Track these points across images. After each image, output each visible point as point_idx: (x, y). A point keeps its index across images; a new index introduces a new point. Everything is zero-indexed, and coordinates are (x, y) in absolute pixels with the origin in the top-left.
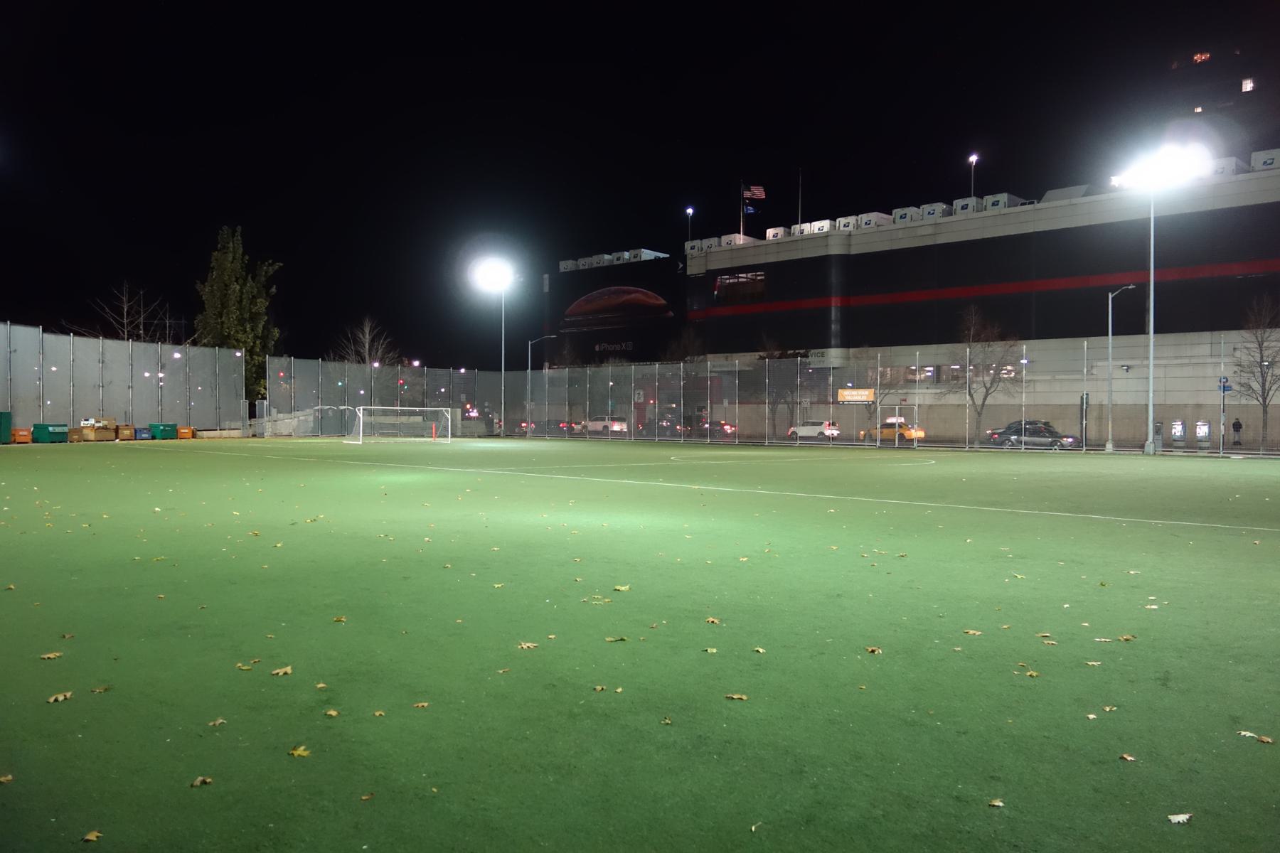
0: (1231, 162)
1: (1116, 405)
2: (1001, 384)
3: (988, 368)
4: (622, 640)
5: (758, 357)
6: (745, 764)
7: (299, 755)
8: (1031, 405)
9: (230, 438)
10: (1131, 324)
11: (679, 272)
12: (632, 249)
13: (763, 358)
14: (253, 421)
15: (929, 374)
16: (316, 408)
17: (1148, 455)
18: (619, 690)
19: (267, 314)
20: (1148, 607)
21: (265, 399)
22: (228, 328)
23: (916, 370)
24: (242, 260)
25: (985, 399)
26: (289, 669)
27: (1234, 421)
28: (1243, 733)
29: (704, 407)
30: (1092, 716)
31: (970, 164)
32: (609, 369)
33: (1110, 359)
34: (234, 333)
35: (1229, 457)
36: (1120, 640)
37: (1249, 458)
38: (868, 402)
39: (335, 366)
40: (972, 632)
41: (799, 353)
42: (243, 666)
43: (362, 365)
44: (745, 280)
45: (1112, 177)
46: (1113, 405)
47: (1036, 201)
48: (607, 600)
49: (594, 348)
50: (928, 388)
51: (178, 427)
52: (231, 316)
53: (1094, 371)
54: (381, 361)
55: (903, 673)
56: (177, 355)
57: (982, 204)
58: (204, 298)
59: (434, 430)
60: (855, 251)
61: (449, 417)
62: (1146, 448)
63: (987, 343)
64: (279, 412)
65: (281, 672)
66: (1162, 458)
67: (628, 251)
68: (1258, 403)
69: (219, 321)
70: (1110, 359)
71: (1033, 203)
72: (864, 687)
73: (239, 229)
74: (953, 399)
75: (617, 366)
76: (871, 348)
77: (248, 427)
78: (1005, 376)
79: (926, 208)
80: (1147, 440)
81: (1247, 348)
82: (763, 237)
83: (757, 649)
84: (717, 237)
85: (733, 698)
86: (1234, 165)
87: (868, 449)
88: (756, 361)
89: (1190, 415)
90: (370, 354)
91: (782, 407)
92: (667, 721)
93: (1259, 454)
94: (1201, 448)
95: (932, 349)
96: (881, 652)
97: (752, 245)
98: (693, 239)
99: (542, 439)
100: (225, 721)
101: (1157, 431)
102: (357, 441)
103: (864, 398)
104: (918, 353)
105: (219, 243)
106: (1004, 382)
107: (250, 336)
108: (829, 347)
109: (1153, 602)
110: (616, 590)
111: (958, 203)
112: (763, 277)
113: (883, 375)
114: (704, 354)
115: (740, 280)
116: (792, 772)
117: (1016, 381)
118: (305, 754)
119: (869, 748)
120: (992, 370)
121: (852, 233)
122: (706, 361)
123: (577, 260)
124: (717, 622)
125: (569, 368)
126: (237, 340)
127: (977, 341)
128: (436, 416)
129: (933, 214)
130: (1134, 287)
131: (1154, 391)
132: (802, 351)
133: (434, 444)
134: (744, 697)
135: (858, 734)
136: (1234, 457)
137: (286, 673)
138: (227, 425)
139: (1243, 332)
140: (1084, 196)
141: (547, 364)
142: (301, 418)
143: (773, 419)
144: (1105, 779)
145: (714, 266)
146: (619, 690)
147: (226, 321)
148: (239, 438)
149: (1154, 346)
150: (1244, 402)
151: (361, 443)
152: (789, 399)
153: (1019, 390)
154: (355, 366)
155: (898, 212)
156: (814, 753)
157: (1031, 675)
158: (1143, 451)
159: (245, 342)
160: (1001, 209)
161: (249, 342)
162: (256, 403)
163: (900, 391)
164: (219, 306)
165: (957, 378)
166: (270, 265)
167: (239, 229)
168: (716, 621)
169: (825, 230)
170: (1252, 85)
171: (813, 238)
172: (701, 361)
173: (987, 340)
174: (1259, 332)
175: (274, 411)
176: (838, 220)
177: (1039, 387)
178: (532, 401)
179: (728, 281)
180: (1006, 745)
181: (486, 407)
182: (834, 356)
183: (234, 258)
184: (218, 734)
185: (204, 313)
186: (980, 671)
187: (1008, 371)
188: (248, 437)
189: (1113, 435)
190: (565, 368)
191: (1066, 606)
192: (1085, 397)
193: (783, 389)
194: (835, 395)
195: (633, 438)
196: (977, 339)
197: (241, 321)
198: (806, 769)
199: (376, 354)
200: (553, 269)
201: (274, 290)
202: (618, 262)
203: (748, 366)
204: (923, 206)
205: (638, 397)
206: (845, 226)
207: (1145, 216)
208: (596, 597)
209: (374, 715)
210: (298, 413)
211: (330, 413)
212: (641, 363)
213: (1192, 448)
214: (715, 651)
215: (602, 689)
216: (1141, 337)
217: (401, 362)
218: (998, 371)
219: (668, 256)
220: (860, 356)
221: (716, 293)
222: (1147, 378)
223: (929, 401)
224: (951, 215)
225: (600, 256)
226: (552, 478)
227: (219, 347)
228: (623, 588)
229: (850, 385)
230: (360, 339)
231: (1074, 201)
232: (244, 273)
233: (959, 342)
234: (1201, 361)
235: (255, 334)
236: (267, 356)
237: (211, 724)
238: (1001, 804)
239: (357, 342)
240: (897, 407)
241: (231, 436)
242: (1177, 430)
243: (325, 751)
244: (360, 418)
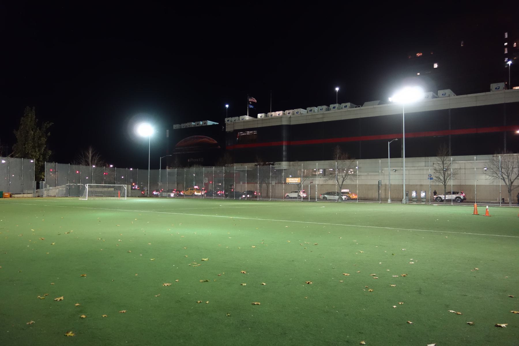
0: (431, 94)
1: (392, 185)
2: (349, 176)
3: (343, 170)
4: (207, 281)
5: (254, 165)
6: (262, 331)
7: (69, 336)
8: (360, 185)
9: (27, 197)
10: (396, 154)
11: (222, 130)
12: (196, 121)
13: (256, 165)
14: (38, 190)
15: (321, 172)
16: (67, 185)
17: (404, 204)
18: (207, 302)
19: (46, 144)
20: (411, 263)
21: (44, 180)
22: (28, 150)
23: (316, 171)
24: (35, 121)
25: (343, 182)
26: (62, 298)
27: (434, 191)
28: (451, 311)
29: (233, 185)
30: (395, 307)
31: (336, 92)
32: (194, 170)
33: (389, 167)
34: (31, 152)
35: (433, 205)
36: (401, 276)
37: (439, 205)
38: (298, 183)
39: (76, 167)
40: (346, 274)
41: (271, 163)
42: (41, 297)
43: (88, 167)
44: (249, 134)
45: (389, 98)
46: (391, 185)
47: (361, 106)
48: (199, 265)
49: (188, 161)
50: (321, 178)
51: (3, 193)
52: (29, 145)
53: (383, 172)
54: (96, 165)
55: (321, 292)
56: (3, 162)
57: (341, 107)
58: (17, 137)
59: (119, 194)
61: (126, 189)
62: (403, 201)
63: (343, 160)
64: (50, 186)
65: (58, 299)
66: (409, 205)
67: (202, 121)
68: (443, 184)
69: (24, 147)
70: (389, 167)
71: (359, 107)
72: (306, 298)
73: (34, 108)
74: (331, 182)
75: (197, 168)
76: (299, 162)
77: (36, 192)
78: (350, 173)
79: (320, 107)
80: (403, 198)
81: (438, 164)
82: (256, 117)
83: (262, 283)
84: (238, 116)
85: (255, 304)
86: (432, 95)
87: (298, 202)
88: (254, 166)
89: (419, 188)
90: (91, 162)
91: (264, 185)
92: (229, 314)
93: (451, 204)
94: (423, 201)
95: (322, 162)
96: (312, 283)
97: (252, 120)
98: (228, 117)
99: (165, 198)
100: (34, 322)
101: (407, 195)
102: (85, 199)
103: (297, 182)
104: (317, 164)
105: (25, 114)
106: (350, 176)
107: (38, 154)
108: (282, 161)
109: (412, 261)
110: (202, 260)
111: (332, 106)
112: (256, 133)
113: (304, 172)
114: (233, 163)
115: (247, 134)
116: (281, 334)
117: (355, 175)
118: (72, 335)
119: (311, 323)
120: (345, 171)
121: (291, 116)
122: (233, 166)
123: (181, 125)
124: (246, 273)
125: (177, 168)
126: (32, 155)
127: (339, 160)
128: (120, 188)
129: (322, 110)
130: (397, 140)
131: (405, 179)
132: (272, 163)
133: (120, 200)
134: (259, 303)
135: (306, 317)
137: (61, 300)
138: (26, 191)
139: (437, 158)
140: (378, 105)
141: (167, 167)
142: (60, 189)
143: (260, 190)
144: (402, 331)
145: (236, 128)
146: (207, 302)
147: (27, 147)
148: (31, 197)
149: (405, 162)
150: (437, 184)
151: (87, 199)
152: (267, 182)
153: (355, 179)
154: (84, 167)
155: (309, 109)
156: (289, 325)
157: (370, 291)
159: (35, 156)
160: (348, 109)
161: (37, 156)
162: (40, 182)
163: (310, 179)
164: (24, 140)
165: (331, 174)
166: (48, 123)
167: (34, 108)
168: (245, 272)
169: (281, 115)
170: (437, 66)
172: (231, 166)
173: (344, 159)
174: (442, 157)
175: (48, 186)
176: (286, 111)
177: (363, 178)
178: (161, 182)
179: (242, 134)
180: (364, 319)
181: (141, 185)
182: (284, 165)
183: (31, 120)
184: (31, 328)
185: (17, 143)
186: (351, 290)
187: (351, 172)
188: (36, 197)
189: (390, 196)
190: (176, 168)
191: (380, 263)
192: (380, 181)
193: (265, 178)
194: (285, 180)
195: (452, 203)
196: (340, 159)
197: (34, 147)
198: (287, 332)
199: (94, 162)
200: (170, 127)
201: (49, 134)
202: (198, 126)
203: (251, 168)
204: (318, 107)
205: (206, 180)
207: (400, 113)
208: (194, 263)
209: (102, 316)
210: (58, 187)
211: (73, 187)
212: (207, 167)
213: (420, 201)
214: (245, 284)
215: (200, 302)
216: (400, 159)
217: (105, 166)
218: (347, 172)
219: (218, 123)
220: (295, 165)
221: (237, 139)
222: (403, 174)
223: (321, 183)
224: (329, 110)
225: (191, 123)
226: (171, 214)
227: (23, 158)
228: (205, 260)
229: (290, 176)
230: (87, 155)
231: (375, 106)
232: (36, 127)
233: (333, 160)
234: (422, 168)
235: (40, 153)
236: (45, 162)
237: (28, 323)
238: (364, 343)
239: (86, 157)
240: (309, 185)
241: (28, 197)
242: (414, 194)
243: (81, 333)
244: (87, 188)
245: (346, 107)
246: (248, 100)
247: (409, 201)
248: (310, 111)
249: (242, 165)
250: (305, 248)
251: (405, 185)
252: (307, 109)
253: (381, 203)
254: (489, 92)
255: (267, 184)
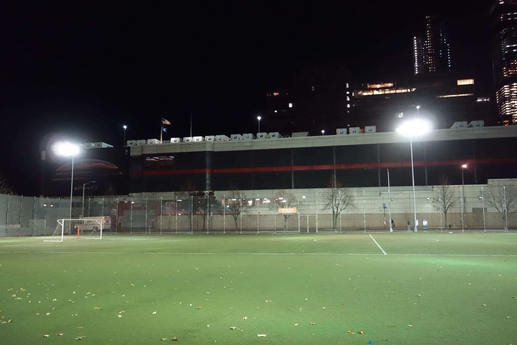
11: (126, 154)
38: (294, 213)
60: (217, 150)
71: (288, 137)
79: (245, 135)
93: (149, 233)
97: (180, 144)
103: (291, 212)
115: (170, 159)
129: (248, 138)
136: (450, 232)
145: (146, 152)
155: (233, 136)
158: (414, 231)
160: (276, 138)
169: (177, 142)
171: (193, 143)
177: (311, 207)
195: (161, 233)
206: (209, 139)
245: (275, 136)
246: (162, 122)
247: (151, 232)
248: (235, 138)
249: (154, 194)
250: (514, 298)
251: (416, 213)
252: (243, 135)
253: (92, 235)
254: (256, 140)
255: (204, 216)
